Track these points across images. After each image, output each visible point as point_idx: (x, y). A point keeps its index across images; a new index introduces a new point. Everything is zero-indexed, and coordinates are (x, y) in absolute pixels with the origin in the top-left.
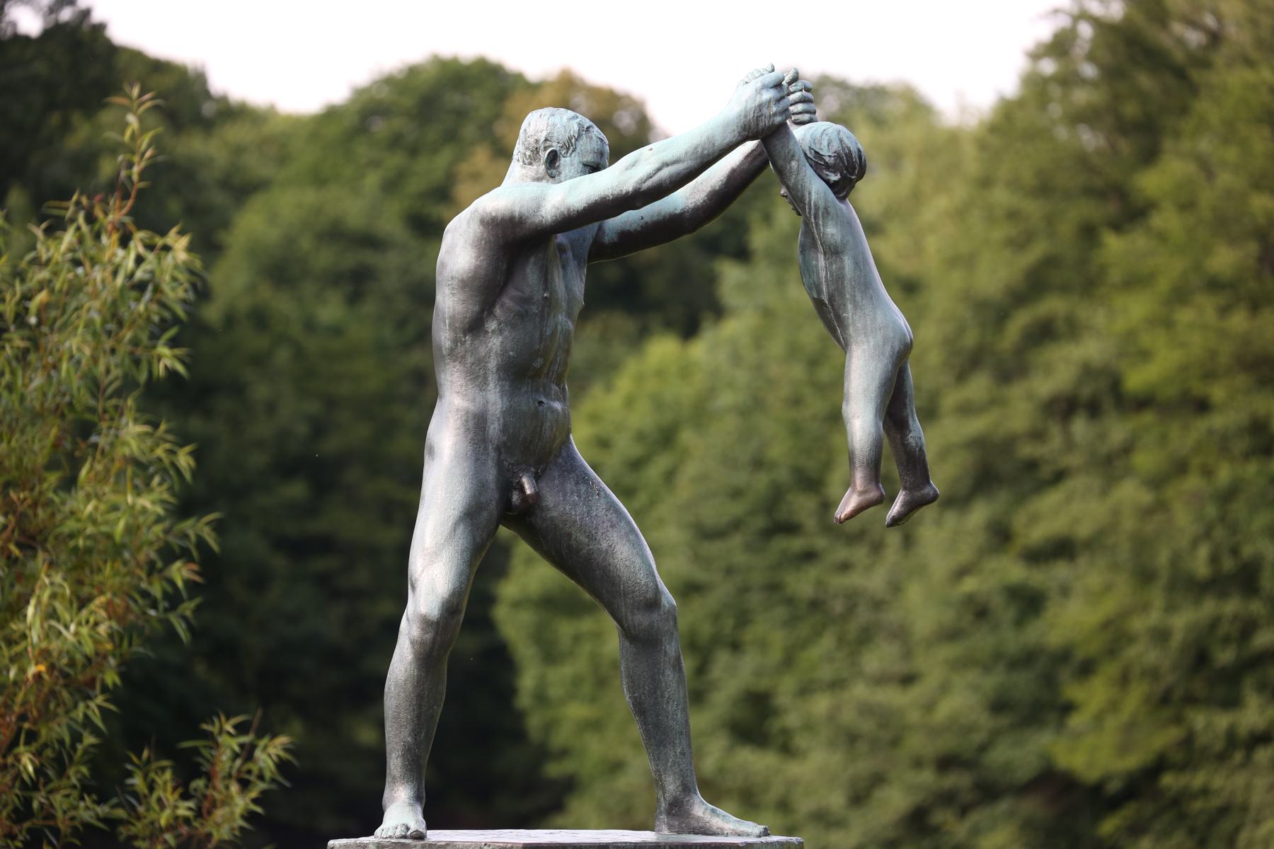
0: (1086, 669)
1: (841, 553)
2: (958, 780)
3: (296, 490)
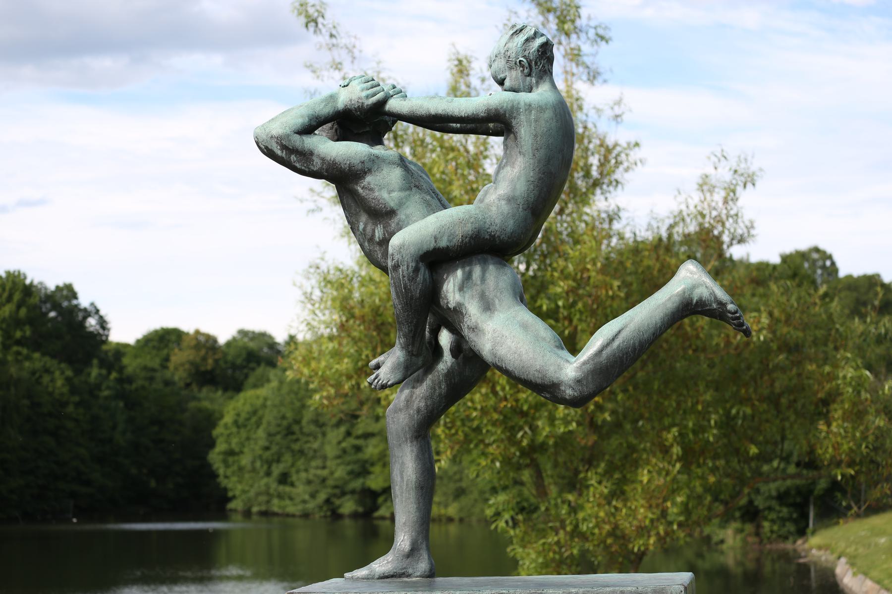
0: (373, 464)
1: (305, 439)
2: (337, 491)
3: (155, 428)
